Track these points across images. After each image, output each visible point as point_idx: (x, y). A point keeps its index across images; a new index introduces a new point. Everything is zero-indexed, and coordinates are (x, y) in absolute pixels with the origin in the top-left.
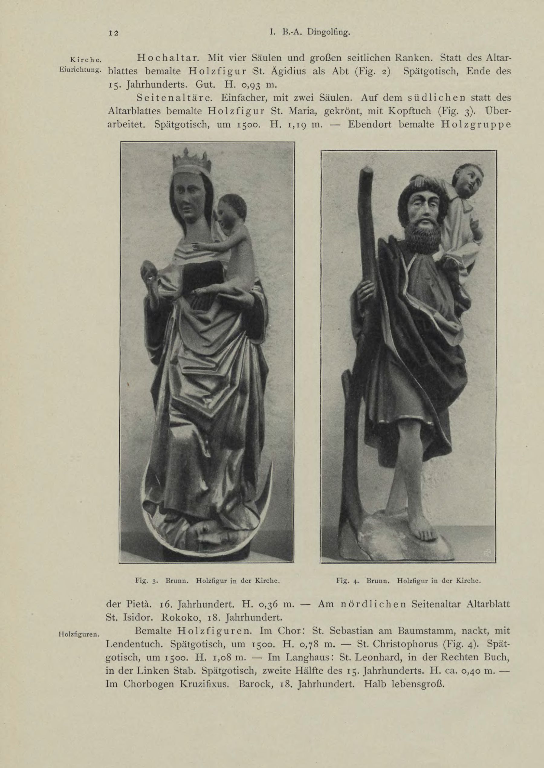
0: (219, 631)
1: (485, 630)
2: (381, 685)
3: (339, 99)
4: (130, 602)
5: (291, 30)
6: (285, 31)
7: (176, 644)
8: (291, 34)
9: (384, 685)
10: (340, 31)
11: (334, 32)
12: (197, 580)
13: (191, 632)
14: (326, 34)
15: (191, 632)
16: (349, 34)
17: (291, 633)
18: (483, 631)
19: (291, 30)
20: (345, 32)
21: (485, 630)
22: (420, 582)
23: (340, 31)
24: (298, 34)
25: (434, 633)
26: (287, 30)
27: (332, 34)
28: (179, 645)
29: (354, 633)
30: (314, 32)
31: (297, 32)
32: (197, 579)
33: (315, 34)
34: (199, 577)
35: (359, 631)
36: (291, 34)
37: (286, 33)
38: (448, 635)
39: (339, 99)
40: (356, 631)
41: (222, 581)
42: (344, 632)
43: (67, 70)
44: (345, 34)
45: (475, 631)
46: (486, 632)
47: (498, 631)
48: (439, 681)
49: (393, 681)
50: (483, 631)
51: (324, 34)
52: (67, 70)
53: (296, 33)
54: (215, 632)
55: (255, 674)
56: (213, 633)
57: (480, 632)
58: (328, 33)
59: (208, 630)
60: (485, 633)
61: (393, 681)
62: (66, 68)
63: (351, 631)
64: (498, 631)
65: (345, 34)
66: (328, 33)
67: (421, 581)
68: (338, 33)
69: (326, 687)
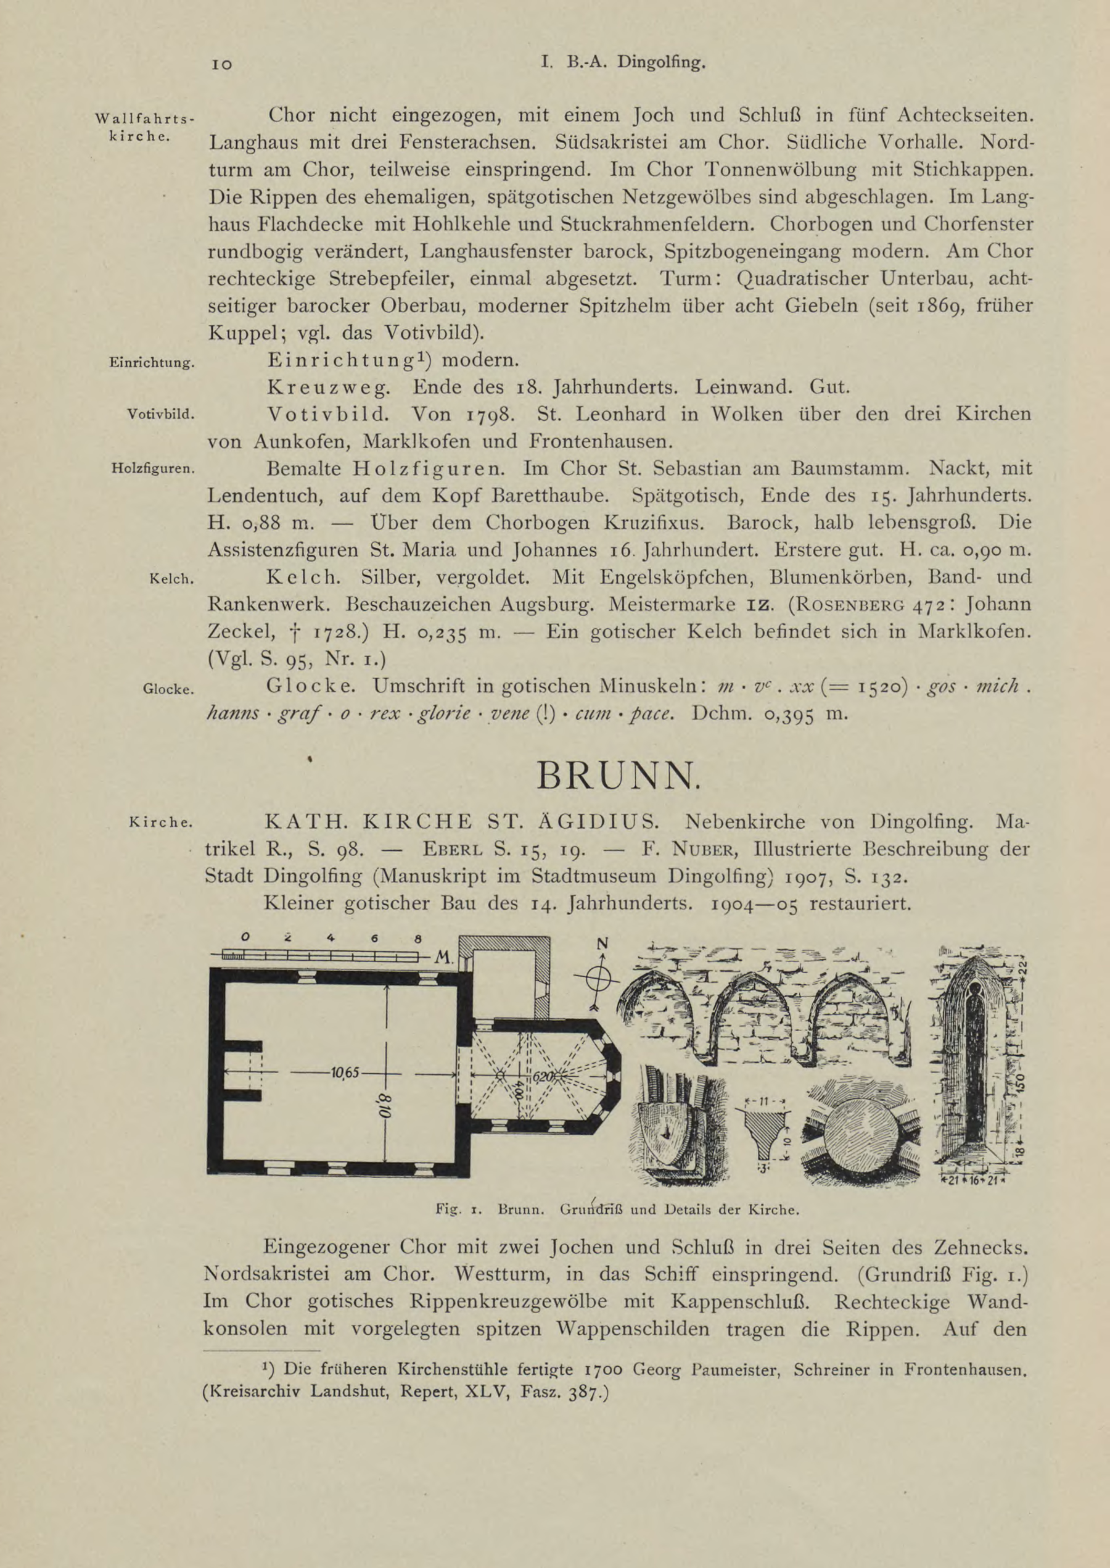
0: (438, 469)
1: (981, 466)
2: (842, 525)
3: (500, 227)
4: (697, 1367)
5: (586, 57)
6: (573, 61)
7: (644, 496)
8: (584, 65)
9: (849, 524)
10: (683, 61)
11: (671, 62)
12: (114, 468)
13: (380, 470)
14: (655, 65)
15: (380, 470)
16: (704, 67)
17: (587, 472)
18: (977, 469)
19: (586, 57)
20: (695, 62)
21: (981, 466)
22: (159, 470)
23: (683, 61)
24: (599, 66)
25: (950, 472)
26: (577, 58)
27: (668, 66)
28: (650, 498)
29: (702, 472)
30: (632, 62)
31: (597, 62)
32: (114, 464)
33: (634, 66)
34: (117, 461)
35: (713, 470)
36: (584, 65)
37: (574, 64)
38: (769, 477)
39: (500, 227)
40: (706, 469)
41: (164, 470)
42: (682, 470)
43: (124, 364)
44: (695, 66)
45: (961, 469)
46: (984, 470)
47: (1008, 470)
48: (966, 517)
49: (871, 515)
50: (977, 469)
51: (650, 65)
52: (124, 364)
53: (595, 65)
54: (431, 471)
55: (319, 503)
56: (426, 474)
57: (971, 471)
58: (661, 63)
59: (416, 467)
60: (981, 473)
61: (871, 515)
62: (124, 360)
63: (697, 470)
64: (1008, 470)
65: (695, 66)
66: (661, 63)
67: (159, 469)
68: (681, 63)
69: (359, 501)
